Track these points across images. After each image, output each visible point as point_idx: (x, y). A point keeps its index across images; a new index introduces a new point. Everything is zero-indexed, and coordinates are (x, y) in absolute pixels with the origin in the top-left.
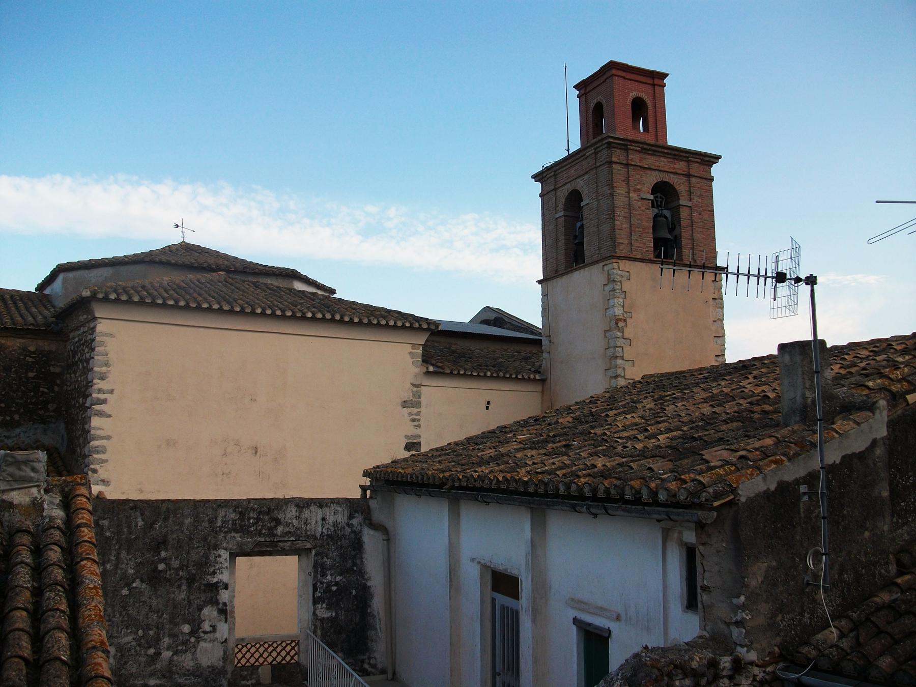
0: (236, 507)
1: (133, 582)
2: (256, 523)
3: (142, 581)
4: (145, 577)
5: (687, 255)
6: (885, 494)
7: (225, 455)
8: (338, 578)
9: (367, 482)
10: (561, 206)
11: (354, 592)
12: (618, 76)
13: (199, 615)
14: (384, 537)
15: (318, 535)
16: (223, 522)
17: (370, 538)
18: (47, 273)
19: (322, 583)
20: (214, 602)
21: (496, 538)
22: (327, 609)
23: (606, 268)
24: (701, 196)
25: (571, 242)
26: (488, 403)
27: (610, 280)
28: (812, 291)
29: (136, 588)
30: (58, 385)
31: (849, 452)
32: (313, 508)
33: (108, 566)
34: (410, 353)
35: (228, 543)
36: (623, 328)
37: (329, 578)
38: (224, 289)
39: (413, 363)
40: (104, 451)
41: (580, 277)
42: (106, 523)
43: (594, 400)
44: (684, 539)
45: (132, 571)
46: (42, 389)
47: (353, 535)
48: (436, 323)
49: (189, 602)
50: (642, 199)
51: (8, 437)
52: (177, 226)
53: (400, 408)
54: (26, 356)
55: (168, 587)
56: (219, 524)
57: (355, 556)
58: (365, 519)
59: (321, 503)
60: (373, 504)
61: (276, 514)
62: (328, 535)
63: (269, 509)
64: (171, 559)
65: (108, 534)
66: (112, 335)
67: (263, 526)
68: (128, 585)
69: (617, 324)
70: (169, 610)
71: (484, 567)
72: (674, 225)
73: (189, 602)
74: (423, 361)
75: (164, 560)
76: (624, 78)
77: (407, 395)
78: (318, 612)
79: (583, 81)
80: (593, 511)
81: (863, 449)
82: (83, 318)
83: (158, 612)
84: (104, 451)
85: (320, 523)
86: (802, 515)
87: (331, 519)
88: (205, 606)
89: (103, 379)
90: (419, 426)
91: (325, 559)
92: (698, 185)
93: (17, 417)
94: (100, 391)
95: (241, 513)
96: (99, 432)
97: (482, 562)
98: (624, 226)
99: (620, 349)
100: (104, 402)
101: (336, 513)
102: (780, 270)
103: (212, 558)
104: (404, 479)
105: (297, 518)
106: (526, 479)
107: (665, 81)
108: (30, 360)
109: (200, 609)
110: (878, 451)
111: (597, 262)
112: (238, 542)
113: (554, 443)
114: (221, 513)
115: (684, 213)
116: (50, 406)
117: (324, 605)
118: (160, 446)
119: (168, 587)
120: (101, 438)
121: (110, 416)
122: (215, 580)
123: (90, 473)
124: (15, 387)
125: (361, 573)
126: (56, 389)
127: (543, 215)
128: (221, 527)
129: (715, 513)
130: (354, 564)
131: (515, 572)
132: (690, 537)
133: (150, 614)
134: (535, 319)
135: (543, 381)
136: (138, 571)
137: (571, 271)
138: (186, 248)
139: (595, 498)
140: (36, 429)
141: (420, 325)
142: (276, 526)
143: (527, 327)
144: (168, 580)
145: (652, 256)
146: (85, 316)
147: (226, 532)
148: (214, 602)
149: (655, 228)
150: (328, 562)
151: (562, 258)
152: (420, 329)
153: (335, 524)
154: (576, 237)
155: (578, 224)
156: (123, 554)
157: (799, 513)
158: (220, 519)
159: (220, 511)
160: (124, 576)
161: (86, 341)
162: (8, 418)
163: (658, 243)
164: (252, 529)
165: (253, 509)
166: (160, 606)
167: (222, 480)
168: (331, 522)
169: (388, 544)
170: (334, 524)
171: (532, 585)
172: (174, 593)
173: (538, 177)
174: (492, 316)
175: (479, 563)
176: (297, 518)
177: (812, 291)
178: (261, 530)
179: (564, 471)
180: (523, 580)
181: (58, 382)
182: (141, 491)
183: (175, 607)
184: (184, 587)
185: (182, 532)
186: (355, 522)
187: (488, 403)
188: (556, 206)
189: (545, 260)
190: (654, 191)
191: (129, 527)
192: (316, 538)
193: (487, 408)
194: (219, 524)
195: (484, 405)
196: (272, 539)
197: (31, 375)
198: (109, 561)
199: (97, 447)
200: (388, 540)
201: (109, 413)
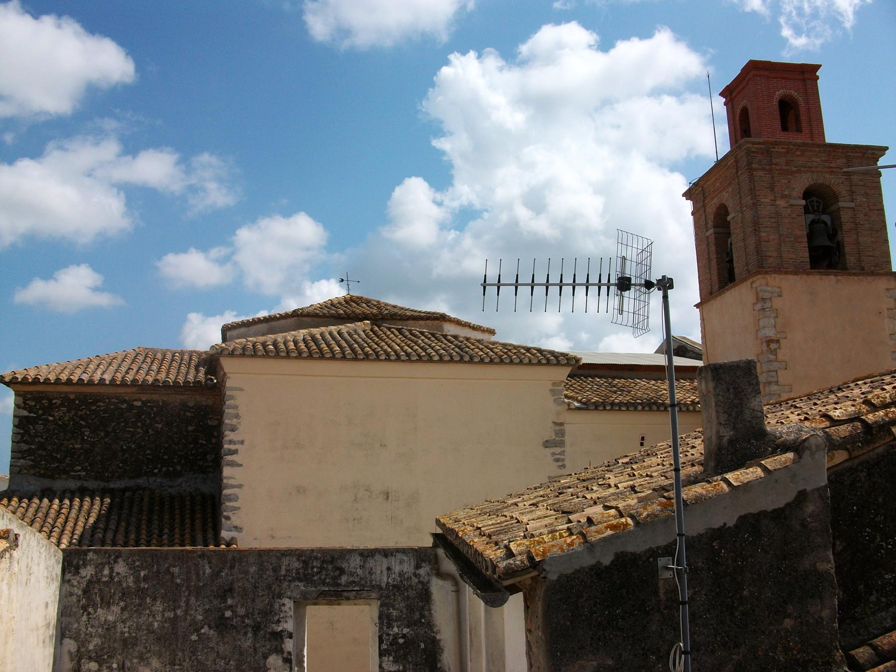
0: (300, 556)
1: (202, 628)
2: (319, 573)
3: (210, 627)
4: (213, 624)
5: (851, 260)
6: (828, 565)
7: (356, 500)
8: (405, 631)
10: (710, 223)
11: (422, 646)
12: (760, 76)
13: (265, 664)
14: (453, 588)
15: (384, 585)
16: (287, 571)
19: (388, 635)
20: (279, 650)
22: (394, 662)
24: (866, 195)
26: (643, 439)
27: (760, 299)
28: (665, 297)
29: (204, 634)
30: (215, 437)
31: (754, 510)
32: (377, 557)
33: (179, 612)
34: (551, 391)
35: (292, 591)
36: (776, 350)
37: (396, 629)
40: (236, 499)
42: (176, 570)
45: (200, 618)
46: (200, 441)
47: (420, 586)
49: (255, 649)
50: (792, 205)
51: (171, 487)
52: (342, 280)
53: (541, 447)
54: (185, 411)
55: (234, 634)
56: (283, 572)
57: (423, 608)
59: (386, 553)
61: (339, 563)
62: (394, 586)
63: (333, 558)
64: (237, 606)
65: (178, 581)
66: (241, 390)
67: (326, 575)
68: (197, 630)
69: (768, 346)
70: (236, 657)
72: (833, 233)
73: (255, 649)
75: (230, 607)
77: (550, 435)
78: (384, 665)
81: (781, 503)
83: (225, 658)
84: (236, 499)
85: (385, 573)
86: (662, 596)
87: (397, 568)
88: (270, 654)
89: (233, 431)
90: (564, 466)
91: (391, 610)
92: (862, 183)
93: (179, 468)
94: (231, 442)
95: (304, 562)
96: (231, 482)
98: (771, 237)
99: (774, 374)
100: (235, 452)
101: (401, 562)
103: (277, 606)
105: (362, 567)
107: (818, 74)
109: (265, 657)
110: (810, 508)
112: (302, 591)
114: (285, 561)
115: (845, 217)
116: (208, 457)
117: (391, 658)
119: (234, 634)
120: (233, 487)
121: (241, 465)
122: (280, 629)
123: (223, 520)
124: (176, 440)
125: (430, 625)
126: (214, 441)
128: (285, 576)
130: (422, 616)
133: (218, 660)
136: (206, 618)
137: (723, 292)
140: (196, 478)
142: (340, 575)
144: (234, 627)
147: (290, 581)
148: (279, 650)
149: (810, 236)
150: (395, 613)
151: (715, 278)
152: (558, 364)
153: (401, 574)
156: (193, 600)
157: (656, 593)
158: (284, 568)
159: (284, 559)
160: (194, 622)
162: (171, 469)
164: (316, 578)
165: (316, 558)
166: (227, 653)
168: (397, 571)
170: (400, 574)
172: (240, 640)
176: (362, 567)
177: (665, 297)
178: (325, 579)
181: (215, 434)
183: (241, 654)
184: (250, 635)
185: (248, 580)
186: (422, 572)
187: (643, 439)
188: (706, 224)
191: (198, 574)
192: (380, 588)
194: (283, 572)
195: (639, 441)
196: (336, 588)
197: (190, 428)
198: (179, 607)
199: (230, 495)
201: (240, 462)
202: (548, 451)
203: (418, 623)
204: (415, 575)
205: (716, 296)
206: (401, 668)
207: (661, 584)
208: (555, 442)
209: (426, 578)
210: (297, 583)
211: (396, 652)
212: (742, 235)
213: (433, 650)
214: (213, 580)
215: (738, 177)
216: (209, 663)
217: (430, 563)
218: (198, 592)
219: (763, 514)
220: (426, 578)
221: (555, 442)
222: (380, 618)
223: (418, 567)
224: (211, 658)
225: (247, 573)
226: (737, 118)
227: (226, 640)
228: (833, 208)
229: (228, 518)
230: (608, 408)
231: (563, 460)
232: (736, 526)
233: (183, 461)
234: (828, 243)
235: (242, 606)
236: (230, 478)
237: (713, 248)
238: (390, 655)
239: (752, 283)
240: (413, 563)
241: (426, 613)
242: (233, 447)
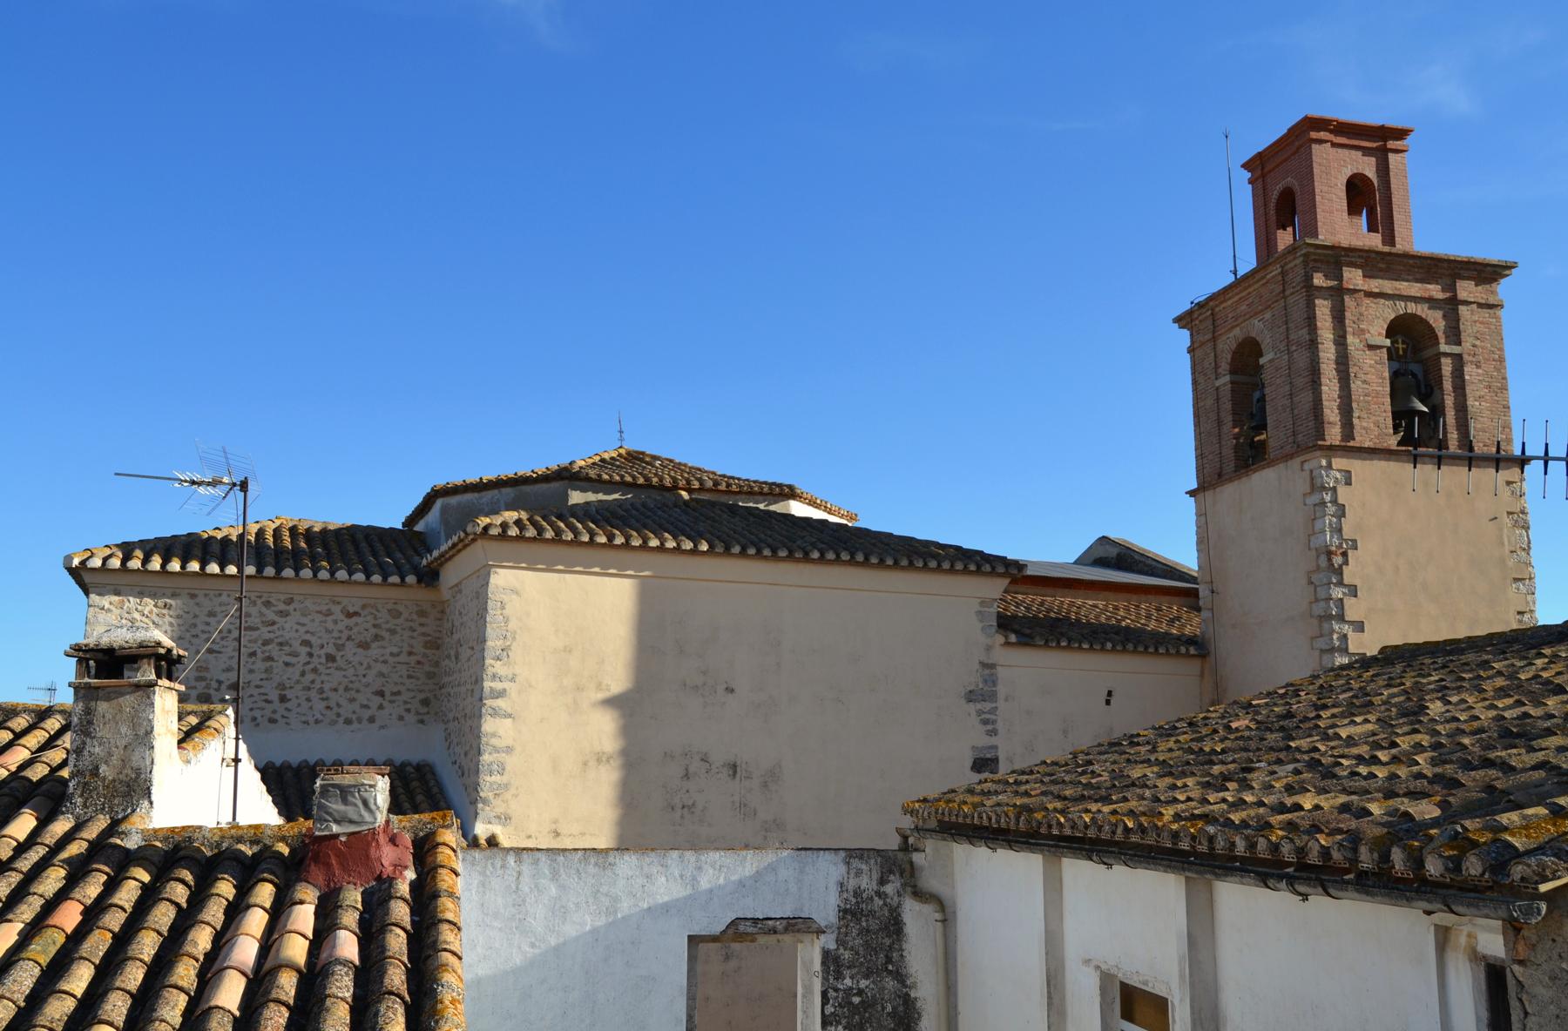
7: (687, 776)
8: (863, 983)
9: (907, 822)
10: (1224, 366)
14: (938, 916)
17: (915, 916)
18: (419, 500)
19: (836, 990)
21: (1127, 917)
23: (1307, 466)
25: (1249, 414)
37: (848, 982)
38: (684, 518)
39: (983, 629)
41: (1264, 480)
43: (1294, 690)
44: (1479, 948)
48: (1019, 566)
53: (963, 701)
58: (904, 885)
71: (1106, 978)
74: (1000, 626)
76: (1334, 145)
77: (973, 679)
79: (1259, 154)
80: (1301, 889)
97: (1104, 967)
100: (501, 694)
104: (968, 821)
106: (1175, 827)
111: (1289, 457)
113: (1223, 763)
118: (585, 764)
125: (900, 976)
127: (1195, 382)
129: (1544, 907)
130: (889, 960)
131: (1160, 990)
132: (1493, 943)
134: (1184, 553)
135: (1198, 647)
139: (1303, 866)
143: (1170, 571)
145: (1392, 442)
151: (1228, 452)
152: (993, 573)
154: (1252, 416)
155: (1257, 395)
163: (1402, 416)
167: (682, 817)
169: (945, 927)
171: (1193, 1013)
173: (1183, 320)
174: (1113, 552)
175: (1098, 967)
179: (1243, 814)
180: (1176, 1003)
182: (557, 834)
186: (889, 889)
187: (1110, 693)
188: (1217, 367)
189: (1200, 456)
190: (1391, 331)
193: (1108, 702)
201: (509, 711)
202: (972, 707)
204: (879, 894)
205: (1231, 480)
208: (982, 694)
209: (896, 899)
212: (1288, 388)
213: (906, 1017)
215: (1285, 297)
217: (901, 875)
221: (982, 694)
223: (882, 881)
226: (1272, 205)
228: (1429, 352)
231: (994, 722)
237: (1227, 405)
238: (839, 1023)
239: (1302, 463)
240: (875, 876)
242: (498, 685)
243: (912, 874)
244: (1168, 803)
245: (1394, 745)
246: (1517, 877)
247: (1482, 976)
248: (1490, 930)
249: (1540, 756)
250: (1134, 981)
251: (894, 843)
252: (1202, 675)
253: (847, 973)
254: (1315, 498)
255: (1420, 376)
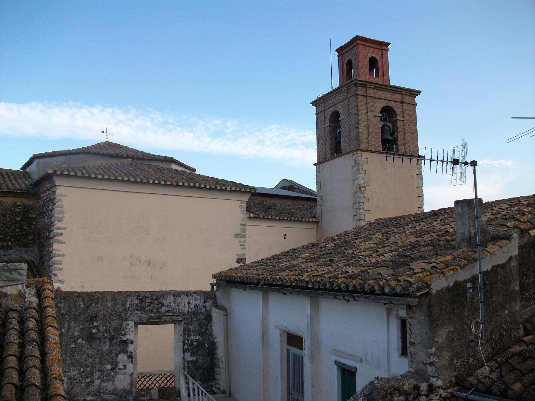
0: (138, 296)
1: (78, 340)
2: (150, 305)
3: (83, 339)
4: (85, 337)
6: (517, 288)
8: (198, 338)
9: (214, 281)
10: (328, 120)
11: (207, 346)
13: (116, 359)
14: (225, 314)
15: (186, 312)
16: (130, 305)
17: (216, 314)
18: (27, 159)
19: (188, 340)
20: (125, 351)
22: (191, 355)
23: (354, 156)
24: (409, 114)
25: (333, 142)
26: (285, 235)
27: (357, 164)
28: (474, 170)
30: (34, 225)
31: (496, 264)
33: (63, 330)
34: (240, 206)
35: (133, 317)
37: (192, 337)
39: (241, 212)
41: (339, 162)
42: (62, 305)
43: (347, 234)
44: (399, 315)
45: (77, 334)
46: (24, 227)
47: (206, 313)
49: (111, 351)
51: (5, 255)
52: (104, 132)
53: (234, 238)
54: (15, 208)
56: (128, 306)
58: (213, 303)
59: (188, 294)
60: (218, 294)
61: (161, 300)
62: (192, 313)
63: (157, 297)
64: (100, 326)
65: (63, 312)
66: (65, 196)
67: (154, 307)
68: (75, 341)
70: (99, 356)
71: (283, 331)
73: (111, 351)
76: (365, 46)
77: (238, 230)
78: (185, 357)
80: (347, 298)
81: (504, 262)
82: (48, 186)
83: (92, 357)
85: (187, 305)
86: (469, 300)
87: (193, 303)
88: (119, 354)
89: (60, 221)
90: (245, 249)
91: (190, 326)
94: (58, 228)
95: (141, 299)
96: (58, 252)
97: (282, 328)
98: (365, 132)
99: (362, 204)
100: (61, 234)
102: (455, 157)
103: (124, 325)
104: (236, 280)
105: (174, 302)
106: (307, 280)
108: (18, 210)
109: (117, 355)
111: (348, 153)
113: (323, 258)
114: (129, 299)
115: (400, 124)
116: (29, 237)
117: (189, 353)
120: (59, 256)
121: (64, 243)
122: (126, 339)
125: (211, 334)
126: (33, 227)
127: (317, 125)
128: (129, 308)
130: (207, 329)
131: (300, 334)
132: (403, 313)
133: (88, 359)
134: (312, 186)
135: (317, 222)
136: (81, 334)
138: (108, 144)
140: (21, 250)
141: (246, 190)
142: (161, 307)
144: (99, 339)
145: (381, 150)
146: (50, 185)
147: (132, 311)
148: (125, 351)
150: (192, 328)
151: (328, 150)
152: (245, 192)
153: (196, 306)
155: (338, 131)
156: (72, 323)
157: (467, 299)
158: (128, 303)
159: (128, 298)
160: (73, 336)
161: (50, 199)
162: (5, 244)
163: (384, 142)
164: (147, 309)
165: (148, 297)
166: (94, 354)
169: (227, 318)
170: (195, 306)
173: (314, 103)
174: (287, 185)
175: (280, 328)
176: (174, 302)
177: (474, 170)
178: (152, 309)
179: (329, 275)
180: (306, 338)
181: (34, 223)
182: (82, 287)
183: (102, 354)
184: (107, 343)
185: (107, 310)
186: (207, 304)
188: (325, 120)
189: (318, 152)
190: (382, 111)
191: (76, 307)
193: (285, 238)
194: (128, 306)
195: (283, 236)
197: (18, 219)
198: (63, 328)
199: (57, 261)
200: (227, 315)
203: (204, 333)
206: (195, 358)
207: (468, 295)
209: (210, 308)
210: (136, 312)
211: (192, 349)
214: (85, 311)
216: (82, 361)
218: (75, 318)
219: (499, 265)
220: (210, 308)
222: (184, 331)
224: (84, 357)
225: (106, 306)
227: (93, 346)
228: (394, 119)
229: (55, 275)
230: (270, 217)
232: (491, 271)
233: (13, 239)
234: (391, 138)
235: (103, 326)
236: (58, 250)
238: (189, 351)
240: (202, 300)
241: (209, 328)
242: (59, 231)
243: (216, 299)
244: (305, 272)
245: (378, 251)
246: (411, 291)
247: (400, 321)
248: (402, 308)
249: (421, 254)
250: (292, 332)
251: (208, 288)
252: (317, 229)
253: (192, 334)
254: (356, 168)
255: (391, 128)
